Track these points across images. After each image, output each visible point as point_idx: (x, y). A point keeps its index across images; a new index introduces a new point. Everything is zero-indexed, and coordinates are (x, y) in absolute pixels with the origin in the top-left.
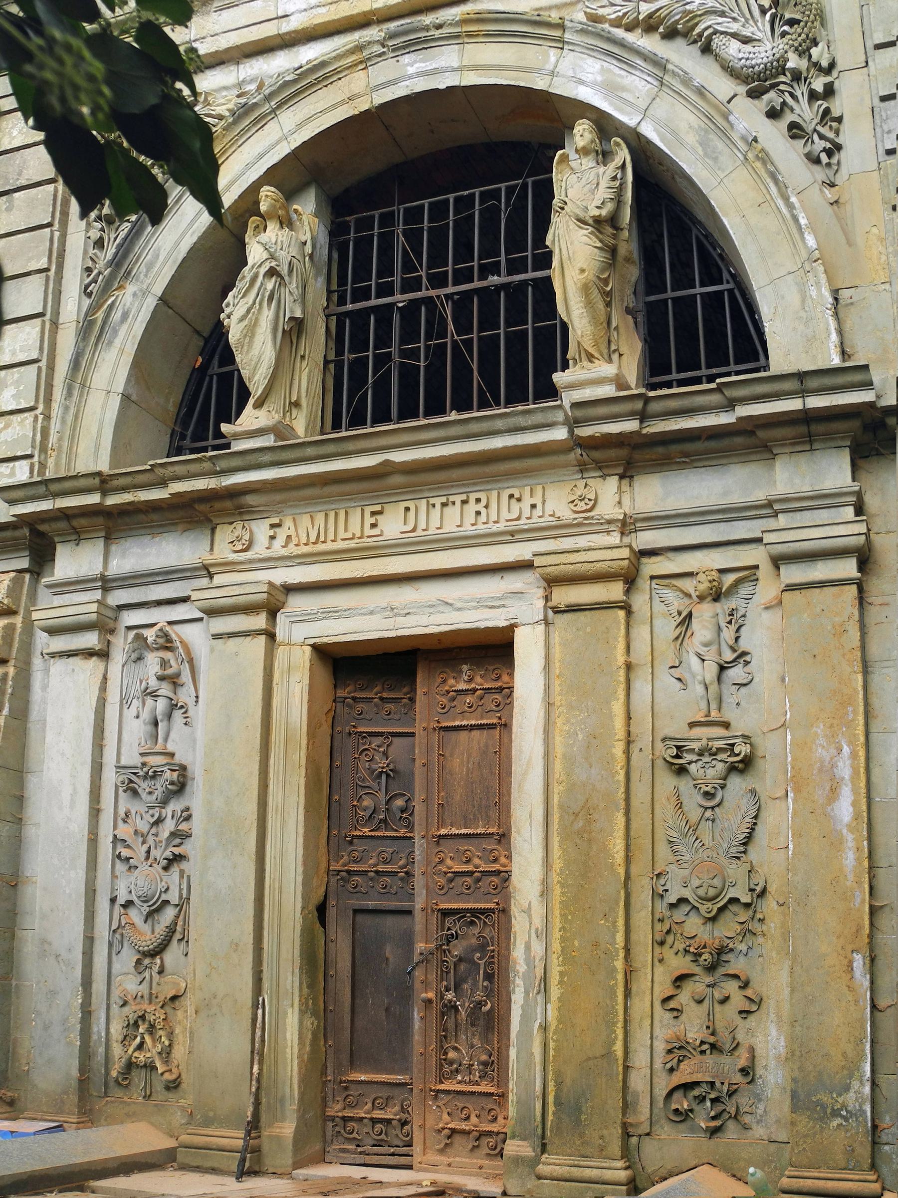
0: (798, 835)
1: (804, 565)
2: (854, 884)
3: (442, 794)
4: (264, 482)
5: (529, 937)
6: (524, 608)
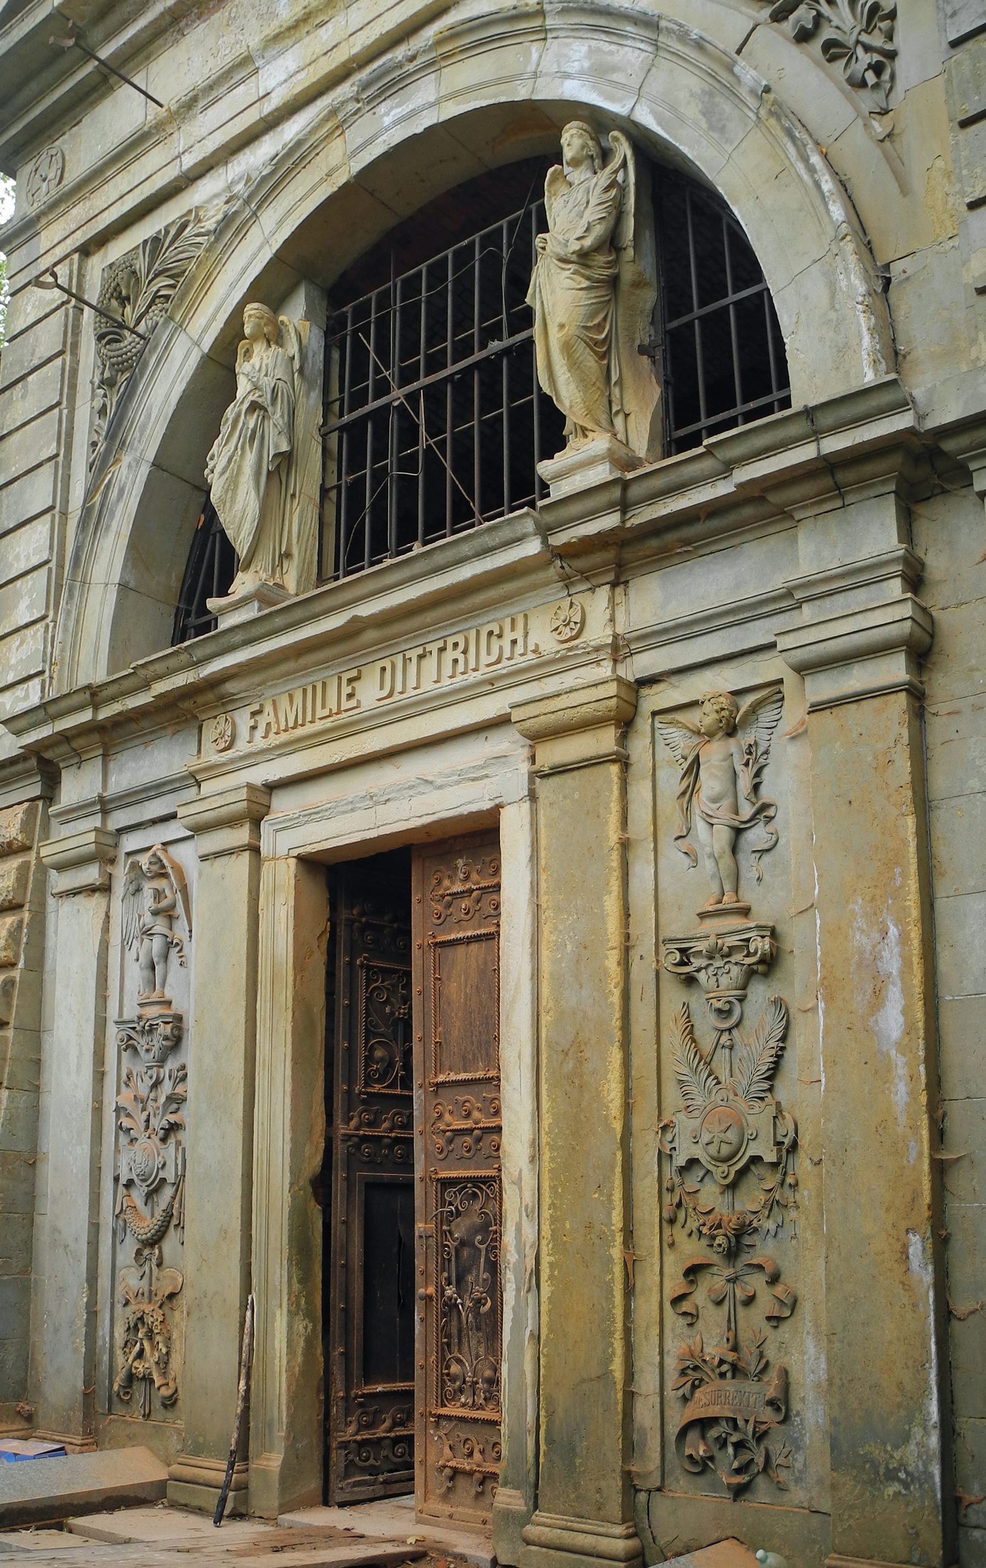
0: (831, 1063)
1: (835, 672)
2: (908, 1130)
3: (440, 1029)
4: (239, 665)
5: (520, 1217)
6: (509, 775)
